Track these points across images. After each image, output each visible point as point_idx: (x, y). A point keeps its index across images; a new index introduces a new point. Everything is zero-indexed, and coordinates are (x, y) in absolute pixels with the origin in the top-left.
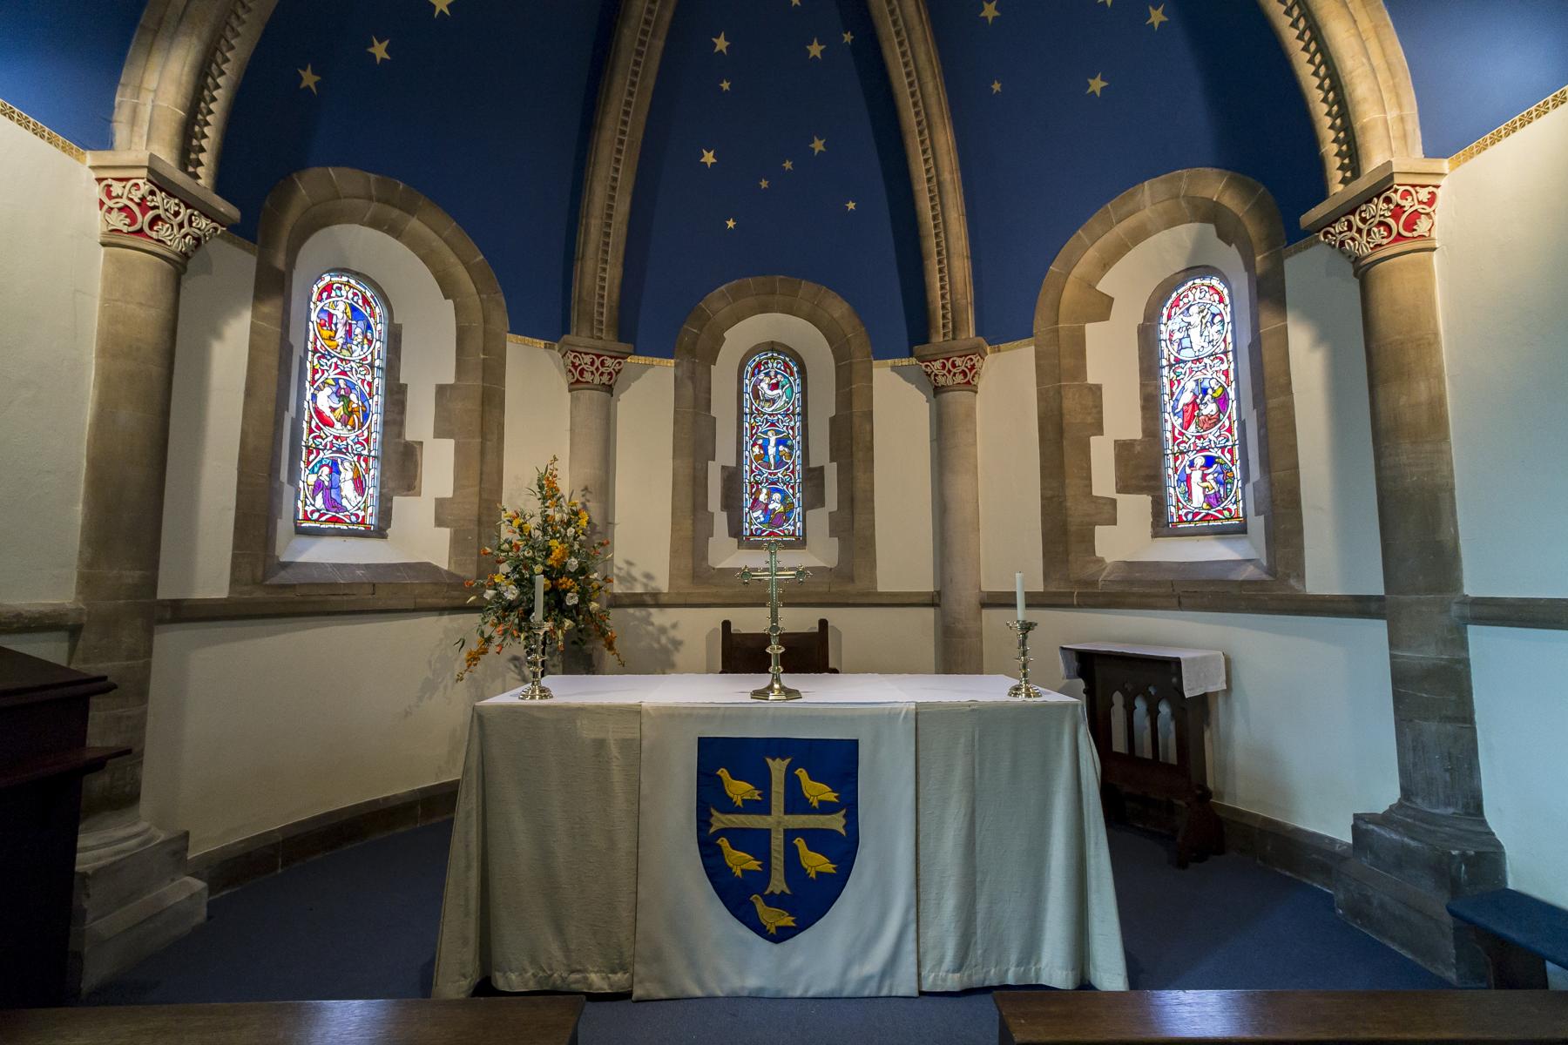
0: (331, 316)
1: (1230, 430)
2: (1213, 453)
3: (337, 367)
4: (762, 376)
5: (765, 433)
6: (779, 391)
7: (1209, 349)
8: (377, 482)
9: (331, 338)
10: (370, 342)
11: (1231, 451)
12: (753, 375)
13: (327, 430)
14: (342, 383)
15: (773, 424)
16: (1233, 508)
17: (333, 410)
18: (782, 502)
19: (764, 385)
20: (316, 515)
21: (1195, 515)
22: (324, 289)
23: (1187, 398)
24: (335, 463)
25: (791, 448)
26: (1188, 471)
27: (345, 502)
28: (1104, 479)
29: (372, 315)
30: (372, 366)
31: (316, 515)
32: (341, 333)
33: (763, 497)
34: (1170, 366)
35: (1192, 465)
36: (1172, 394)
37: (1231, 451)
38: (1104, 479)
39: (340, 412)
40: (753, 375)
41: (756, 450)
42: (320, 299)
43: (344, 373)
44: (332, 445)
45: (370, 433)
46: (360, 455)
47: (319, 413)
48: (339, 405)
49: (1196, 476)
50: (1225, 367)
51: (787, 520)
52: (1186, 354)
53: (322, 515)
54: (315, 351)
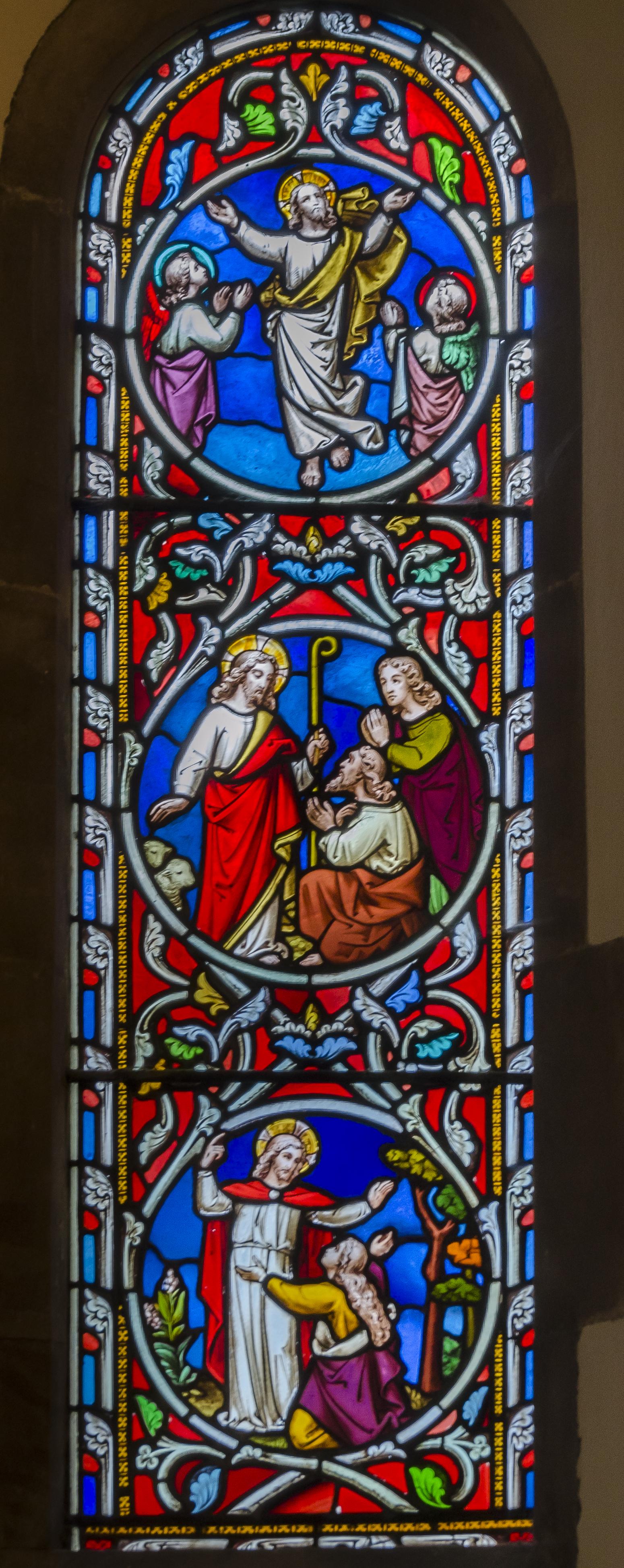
1: (479, 982)
2: (371, 1109)
7: (387, 471)
11: (479, 1120)
16: (468, 1451)
21: (240, 1478)
23: (227, 733)
26: (212, 1198)
30: (481, 514)
34: (140, 511)
35: (237, 1165)
36: (142, 693)
37: (479, 1120)
49: (262, 1233)
50: (472, 594)
52: (239, 460)
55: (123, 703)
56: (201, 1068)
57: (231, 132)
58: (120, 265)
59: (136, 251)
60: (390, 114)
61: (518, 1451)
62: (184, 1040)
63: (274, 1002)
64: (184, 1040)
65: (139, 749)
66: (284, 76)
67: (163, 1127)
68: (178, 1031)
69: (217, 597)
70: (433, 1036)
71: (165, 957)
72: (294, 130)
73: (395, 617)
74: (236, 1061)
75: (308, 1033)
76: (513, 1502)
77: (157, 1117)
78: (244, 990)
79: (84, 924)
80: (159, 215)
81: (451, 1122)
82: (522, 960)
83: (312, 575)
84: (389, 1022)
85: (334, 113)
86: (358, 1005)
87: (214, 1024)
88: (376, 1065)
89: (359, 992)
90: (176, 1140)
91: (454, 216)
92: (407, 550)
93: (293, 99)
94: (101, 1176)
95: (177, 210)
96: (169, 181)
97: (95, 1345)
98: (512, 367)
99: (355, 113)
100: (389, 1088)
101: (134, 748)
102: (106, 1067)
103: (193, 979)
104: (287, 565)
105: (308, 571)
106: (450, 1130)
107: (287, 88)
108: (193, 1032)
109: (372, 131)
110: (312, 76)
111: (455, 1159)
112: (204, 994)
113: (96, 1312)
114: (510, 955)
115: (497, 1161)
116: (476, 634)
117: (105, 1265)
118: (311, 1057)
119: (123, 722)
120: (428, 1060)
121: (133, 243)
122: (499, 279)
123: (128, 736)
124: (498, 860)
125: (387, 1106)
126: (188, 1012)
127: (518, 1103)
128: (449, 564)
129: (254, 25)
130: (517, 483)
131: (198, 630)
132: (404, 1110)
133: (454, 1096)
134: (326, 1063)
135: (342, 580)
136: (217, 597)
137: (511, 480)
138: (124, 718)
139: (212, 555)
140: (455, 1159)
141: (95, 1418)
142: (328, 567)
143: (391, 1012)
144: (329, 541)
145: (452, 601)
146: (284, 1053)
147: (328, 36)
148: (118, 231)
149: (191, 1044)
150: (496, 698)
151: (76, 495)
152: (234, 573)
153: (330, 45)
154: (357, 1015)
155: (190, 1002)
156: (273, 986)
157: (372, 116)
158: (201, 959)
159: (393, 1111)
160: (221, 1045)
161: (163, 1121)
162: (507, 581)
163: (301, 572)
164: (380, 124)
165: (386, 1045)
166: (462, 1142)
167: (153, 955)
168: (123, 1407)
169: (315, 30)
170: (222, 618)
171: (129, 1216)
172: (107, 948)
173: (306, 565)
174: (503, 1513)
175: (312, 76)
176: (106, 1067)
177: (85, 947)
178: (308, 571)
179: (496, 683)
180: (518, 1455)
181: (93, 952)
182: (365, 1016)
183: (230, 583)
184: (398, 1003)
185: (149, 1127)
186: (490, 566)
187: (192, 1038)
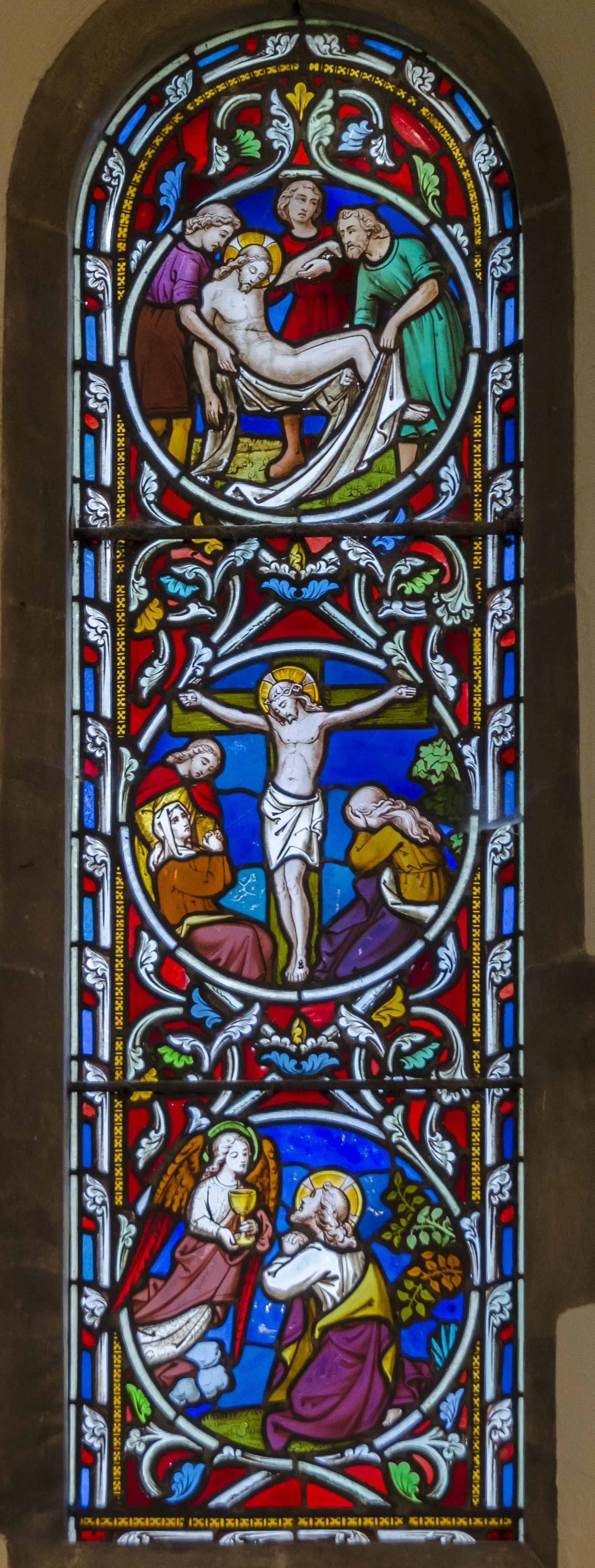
1: (458, 999)
4: (213, 224)
5: (242, 684)
6: (352, 345)
11: (456, 1123)
12: (145, 220)
15: (302, 618)
18: (370, 1240)
19: (233, 301)
20: (188, 1477)
25: (445, 803)
31: (188, 1477)
33: (214, 1203)
37: (456, 1123)
40: (145, 220)
41: (169, 824)
51: (415, 1381)
56: (192, 1078)
57: (221, 160)
58: (115, 288)
59: (131, 278)
60: (376, 134)
61: (497, 1096)
62: (179, 1050)
63: (264, 1017)
64: (180, 578)
65: (136, 764)
66: (274, 97)
69: (209, 613)
70: (416, 572)
71: (161, 501)
72: (282, 149)
73: (379, 631)
74: (224, 1074)
75: (293, 1048)
76: (491, 1501)
78: (236, 1004)
79: (84, 484)
80: (156, 240)
81: (433, 1134)
82: (501, 502)
83: (298, 1067)
84: (375, 1037)
85: (320, 128)
86: (342, 1022)
93: (282, 120)
94: (99, 845)
95: (173, 234)
96: (163, 202)
99: (341, 128)
101: (130, 764)
105: (294, 589)
106: (431, 1141)
107: (276, 107)
108: (187, 1042)
109: (359, 148)
110: (300, 96)
113: (94, 1198)
114: (488, 1428)
115: (477, 701)
116: (458, 645)
117: (102, 1157)
118: (299, 1071)
121: (128, 267)
122: (480, 288)
128: (434, 576)
130: (499, 378)
131: (189, 649)
132: (389, 1122)
134: (312, 606)
135: (329, 596)
136: (209, 613)
137: (493, 490)
138: (119, 1201)
140: (440, 1171)
141: (93, 1412)
142: (313, 584)
143: (376, 1026)
144: (314, 1031)
146: (273, 1067)
149: (187, 583)
150: (476, 947)
151: (77, 526)
154: (343, 1031)
159: (378, 652)
160: (212, 1058)
162: (488, 593)
163: (289, 591)
167: (146, 970)
168: (117, 1401)
169: (301, 53)
170: (215, 638)
171: (123, 1219)
172: (107, 628)
173: (292, 1055)
174: (483, 1511)
175: (300, 96)
176: (103, 1079)
177: (87, 393)
178: (294, 589)
179: (476, 933)
182: (351, 1033)
184: (384, 1019)
187: (187, 1048)
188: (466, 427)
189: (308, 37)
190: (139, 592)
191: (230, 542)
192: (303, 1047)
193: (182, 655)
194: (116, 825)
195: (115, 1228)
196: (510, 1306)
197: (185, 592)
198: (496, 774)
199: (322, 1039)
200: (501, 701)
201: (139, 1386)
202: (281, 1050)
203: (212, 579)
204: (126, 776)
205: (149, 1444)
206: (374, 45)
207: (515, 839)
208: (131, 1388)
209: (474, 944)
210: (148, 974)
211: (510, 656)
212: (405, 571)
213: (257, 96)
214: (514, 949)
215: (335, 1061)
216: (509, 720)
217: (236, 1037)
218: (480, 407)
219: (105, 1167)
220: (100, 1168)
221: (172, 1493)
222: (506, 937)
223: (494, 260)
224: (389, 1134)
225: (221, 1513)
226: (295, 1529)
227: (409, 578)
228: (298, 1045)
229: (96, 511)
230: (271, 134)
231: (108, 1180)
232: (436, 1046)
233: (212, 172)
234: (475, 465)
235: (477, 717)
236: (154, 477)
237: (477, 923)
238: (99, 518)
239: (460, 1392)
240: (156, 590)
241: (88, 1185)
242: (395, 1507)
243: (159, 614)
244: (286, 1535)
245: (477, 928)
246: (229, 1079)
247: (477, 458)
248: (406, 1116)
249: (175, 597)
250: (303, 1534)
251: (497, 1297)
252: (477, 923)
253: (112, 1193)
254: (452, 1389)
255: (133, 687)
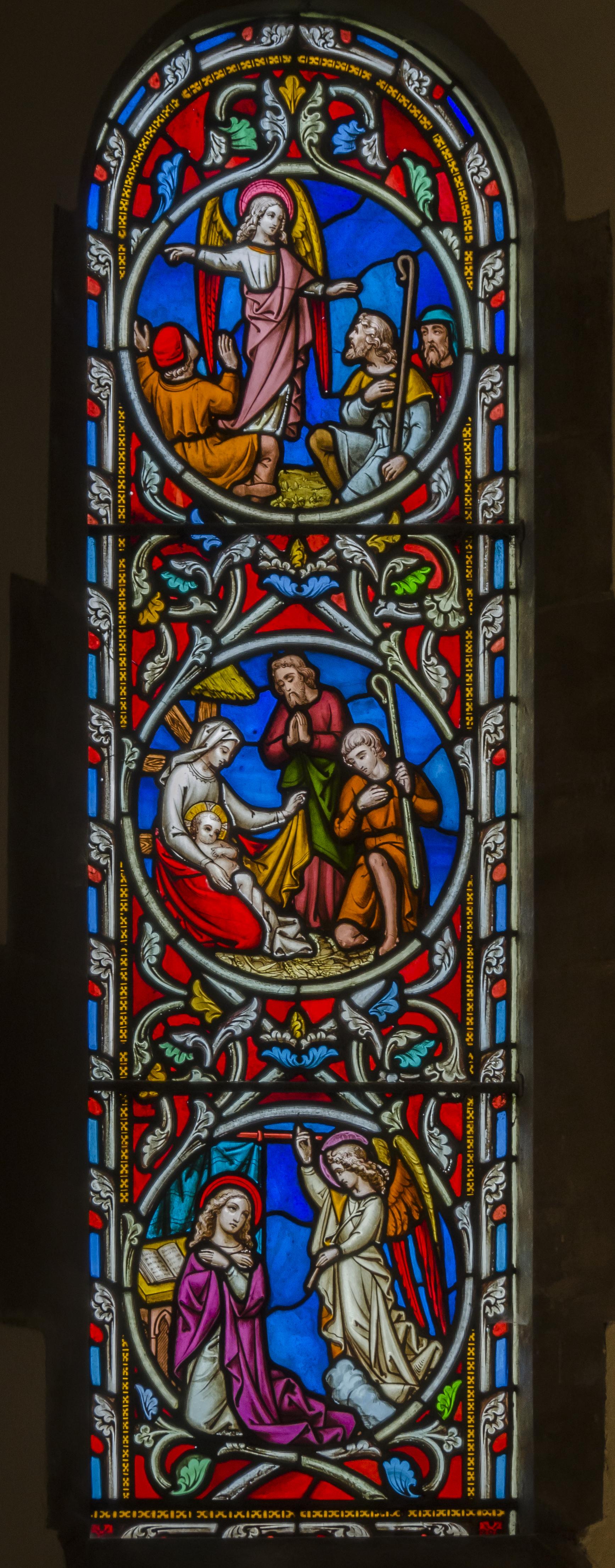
0: (210, 283)
3: (258, 584)
8: (518, 1245)
9: (217, 425)
10: (441, 383)
12: (142, 214)
13: (231, 975)
14: (290, 677)
17: (248, 846)
20: (194, 1471)
22: (166, 140)
24: (273, 1146)
27: (347, 1382)
28: (180, 917)
29: (446, 211)
30: (458, 528)
31: (194, 1471)
32: (270, 373)
38: (180, 917)
39: (294, 849)
42: (144, 210)
43: (300, 612)
44: (259, 1060)
45: (469, 945)
46: (415, 1091)
47: (176, 878)
48: (281, 817)
53: (223, 1470)
54: (136, 523)
55: (125, 1412)
57: (216, 154)
59: (131, 259)
60: (368, 133)
62: (180, 574)
63: (263, 1013)
64: (180, 574)
67: (163, 1129)
68: (178, 1038)
69: (210, 608)
70: (409, 571)
73: (376, 632)
77: (157, 647)
78: (237, 998)
83: (300, 589)
87: (209, 1031)
88: (360, 1076)
89: (344, 1005)
90: (173, 1143)
91: (427, 232)
92: (390, 1035)
95: (169, 222)
97: (97, 413)
98: (483, 390)
100: (371, 1096)
101: (132, 753)
102: (108, 1076)
103: (188, 987)
104: (275, 1052)
108: (191, 1038)
110: (292, 88)
111: (433, 694)
112: (201, 1002)
119: (124, 1203)
120: (410, 1070)
121: (128, 252)
123: (129, 1217)
124: (470, 284)
125: (369, 641)
126: (186, 1019)
127: (489, 994)
129: (238, 39)
132: (384, 646)
133: (432, 1104)
135: (326, 595)
136: (210, 608)
138: (124, 1198)
139: (204, 569)
140: (433, 694)
142: (312, 581)
143: (373, 1020)
145: (431, 615)
147: (311, 52)
148: (113, 241)
152: (225, 582)
153: (314, 60)
154: (339, 553)
155: (187, 1009)
156: (264, 997)
157: (350, 135)
158: (198, 971)
159: (375, 649)
161: (163, 1125)
162: (481, 602)
163: (287, 586)
164: (357, 140)
165: (368, 580)
166: (438, 676)
167: (150, 493)
169: (296, 45)
175: (292, 88)
178: (294, 1057)
180: (486, 408)
181: (94, 259)
183: (221, 595)
185: (150, 657)
186: (465, 584)
187: (189, 572)
188: (461, 900)
189: (303, 30)
190: (142, 586)
191: (229, 537)
192: (303, 572)
193: (184, 648)
194: (119, 815)
195: (122, 1226)
196: (503, 846)
197: (184, 587)
198: (487, 661)
199: (321, 564)
200: (492, 476)
201: (148, 1384)
202: (283, 1045)
203: (211, 573)
204: (131, 1240)
205: (157, 1438)
206: (367, 41)
207: (509, 1413)
208: (139, 1388)
209: (467, 704)
210: (152, 495)
211: (500, 314)
212: (402, 1043)
213: (252, 87)
214: (507, 832)
215: (334, 1052)
216: (500, 493)
217: (238, 1032)
218: (470, 419)
219: (109, 465)
220: (109, 1389)
221: (178, 1488)
222: (499, 1161)
223: (488, 1299)
224: (384, 657)
225: (227, 1505)
226: (297, 1520)
227: (404, 1051)
228: (299, 1040)
229: (98, 845)
230: (265, 124)
231: (114, 1176)
232: (431, 1044)
233: (208, 163)
234: (469, 1354)
235: (469, 720)
236: (156, 468)
237: (472, 1370)
238: (100, 852)
239: (457, 1384)
240: (158, 584)
241: (94, 1066)
242: (396, 1504)
243: (161, 606)
244: (290, 1527)
245: (471, 1376)
246: (232, 1080)
247: (471, 1347)
248: (404, 1111)
249: (176, 592)
250: (307, 1527)
251: (490, 610)
252: (472, 1370)
253: (117, 1190)
254: (448, 1381)
255: (135, 1156)
